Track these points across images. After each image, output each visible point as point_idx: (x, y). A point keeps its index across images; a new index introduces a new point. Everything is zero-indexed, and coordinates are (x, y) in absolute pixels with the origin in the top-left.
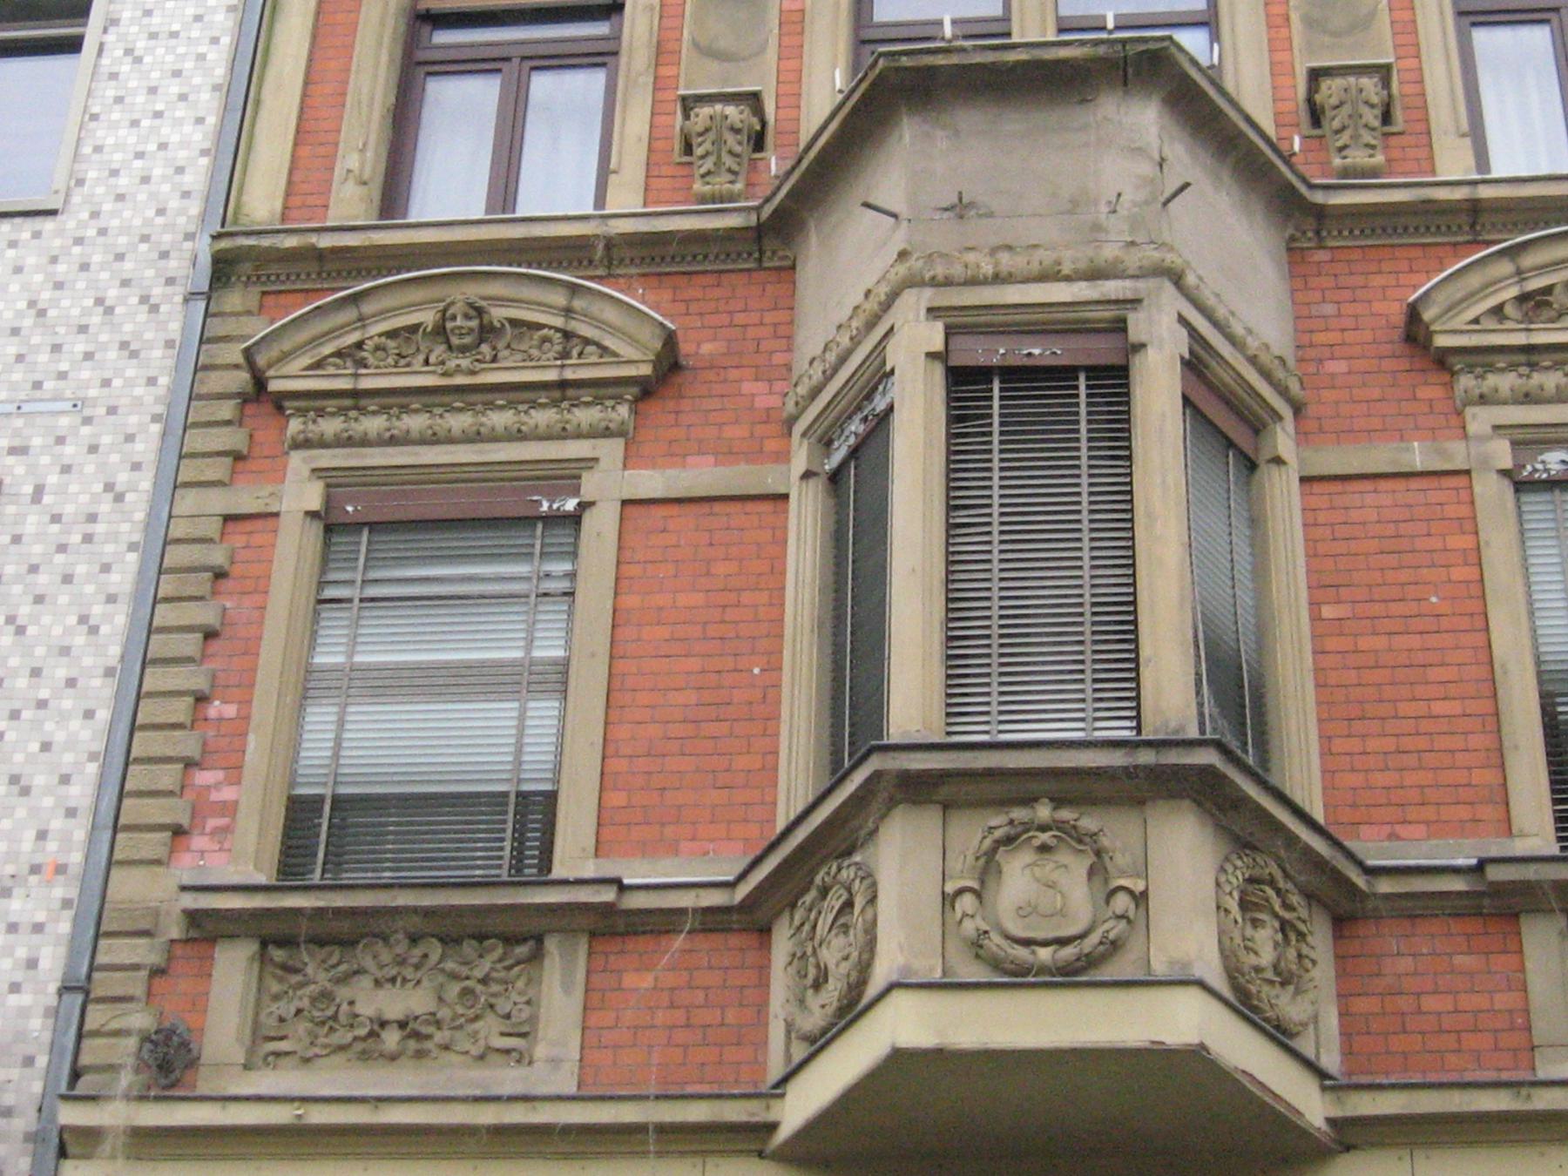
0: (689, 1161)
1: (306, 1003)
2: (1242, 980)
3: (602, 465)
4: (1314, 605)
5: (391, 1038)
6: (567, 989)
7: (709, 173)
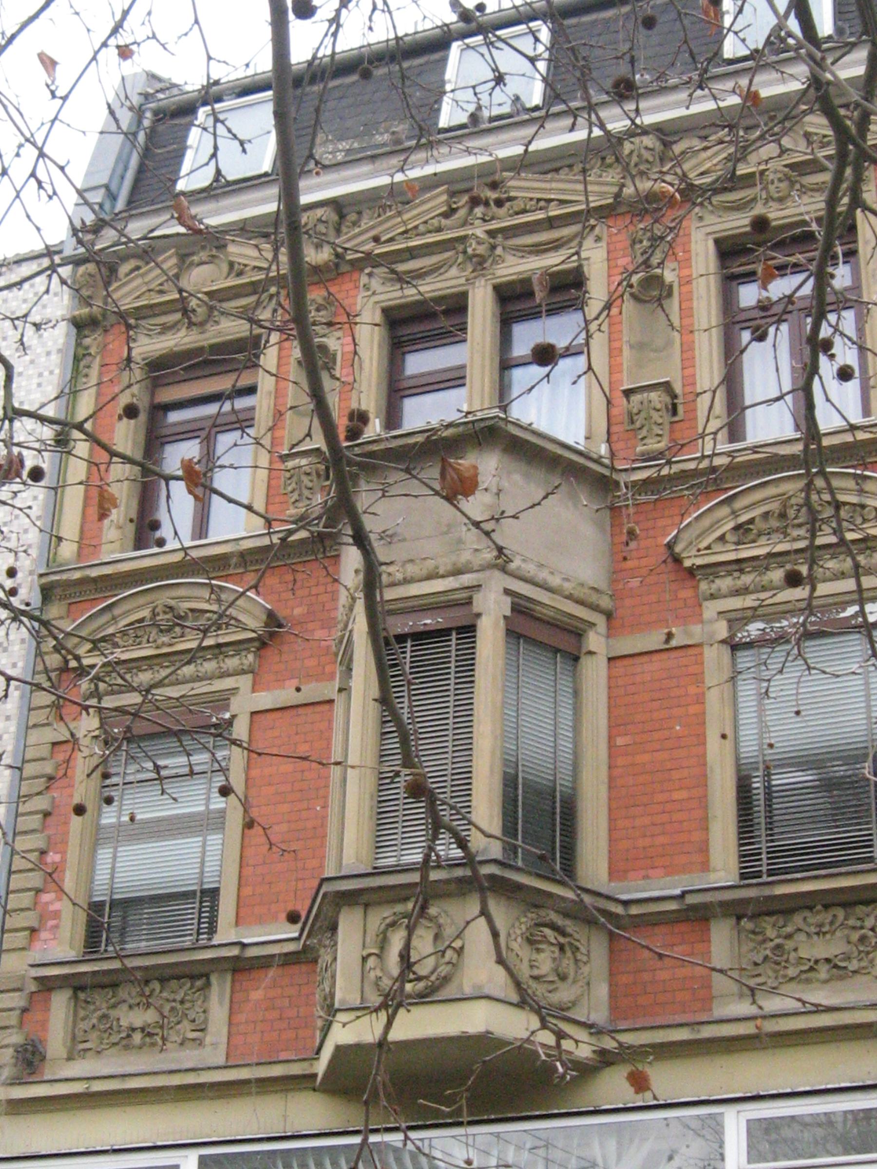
0: (278, 1096)
1: (95, 1021)
3: (241, 691)
4: (611, 739)
5: (137, 1037)
6: (221, 1003)
7: (297, 501)
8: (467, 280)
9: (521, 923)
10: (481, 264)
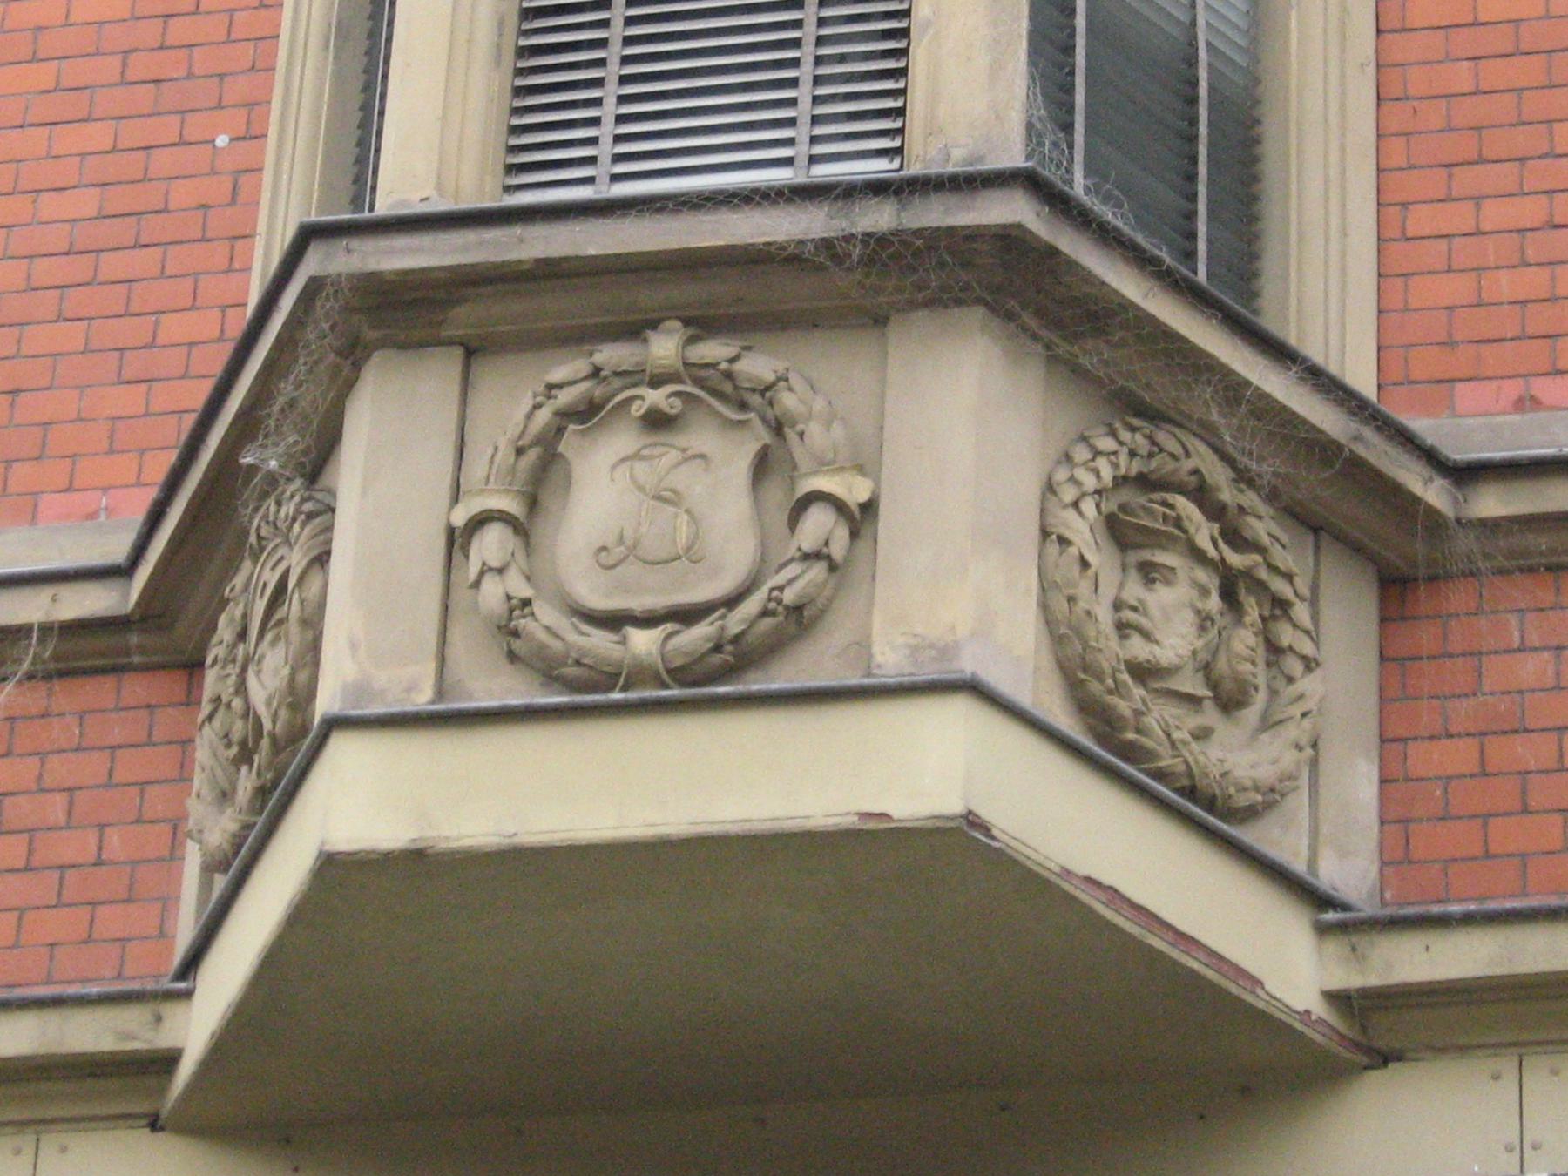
2: (1095, 687)
9: (1097, 453)
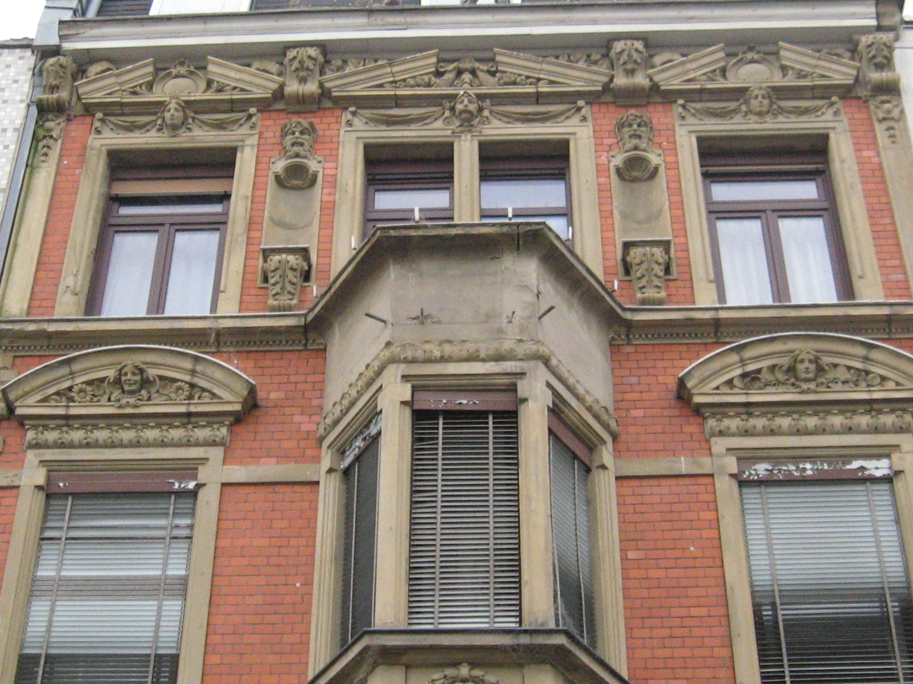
3: (210, 463)
4: (623, 551)
7: (277, 294)
8: (453, 133)
10: (468, 120)
